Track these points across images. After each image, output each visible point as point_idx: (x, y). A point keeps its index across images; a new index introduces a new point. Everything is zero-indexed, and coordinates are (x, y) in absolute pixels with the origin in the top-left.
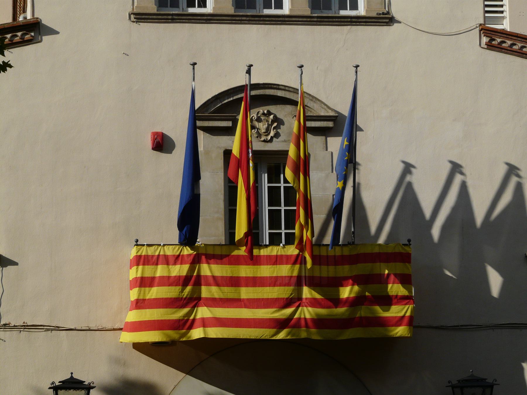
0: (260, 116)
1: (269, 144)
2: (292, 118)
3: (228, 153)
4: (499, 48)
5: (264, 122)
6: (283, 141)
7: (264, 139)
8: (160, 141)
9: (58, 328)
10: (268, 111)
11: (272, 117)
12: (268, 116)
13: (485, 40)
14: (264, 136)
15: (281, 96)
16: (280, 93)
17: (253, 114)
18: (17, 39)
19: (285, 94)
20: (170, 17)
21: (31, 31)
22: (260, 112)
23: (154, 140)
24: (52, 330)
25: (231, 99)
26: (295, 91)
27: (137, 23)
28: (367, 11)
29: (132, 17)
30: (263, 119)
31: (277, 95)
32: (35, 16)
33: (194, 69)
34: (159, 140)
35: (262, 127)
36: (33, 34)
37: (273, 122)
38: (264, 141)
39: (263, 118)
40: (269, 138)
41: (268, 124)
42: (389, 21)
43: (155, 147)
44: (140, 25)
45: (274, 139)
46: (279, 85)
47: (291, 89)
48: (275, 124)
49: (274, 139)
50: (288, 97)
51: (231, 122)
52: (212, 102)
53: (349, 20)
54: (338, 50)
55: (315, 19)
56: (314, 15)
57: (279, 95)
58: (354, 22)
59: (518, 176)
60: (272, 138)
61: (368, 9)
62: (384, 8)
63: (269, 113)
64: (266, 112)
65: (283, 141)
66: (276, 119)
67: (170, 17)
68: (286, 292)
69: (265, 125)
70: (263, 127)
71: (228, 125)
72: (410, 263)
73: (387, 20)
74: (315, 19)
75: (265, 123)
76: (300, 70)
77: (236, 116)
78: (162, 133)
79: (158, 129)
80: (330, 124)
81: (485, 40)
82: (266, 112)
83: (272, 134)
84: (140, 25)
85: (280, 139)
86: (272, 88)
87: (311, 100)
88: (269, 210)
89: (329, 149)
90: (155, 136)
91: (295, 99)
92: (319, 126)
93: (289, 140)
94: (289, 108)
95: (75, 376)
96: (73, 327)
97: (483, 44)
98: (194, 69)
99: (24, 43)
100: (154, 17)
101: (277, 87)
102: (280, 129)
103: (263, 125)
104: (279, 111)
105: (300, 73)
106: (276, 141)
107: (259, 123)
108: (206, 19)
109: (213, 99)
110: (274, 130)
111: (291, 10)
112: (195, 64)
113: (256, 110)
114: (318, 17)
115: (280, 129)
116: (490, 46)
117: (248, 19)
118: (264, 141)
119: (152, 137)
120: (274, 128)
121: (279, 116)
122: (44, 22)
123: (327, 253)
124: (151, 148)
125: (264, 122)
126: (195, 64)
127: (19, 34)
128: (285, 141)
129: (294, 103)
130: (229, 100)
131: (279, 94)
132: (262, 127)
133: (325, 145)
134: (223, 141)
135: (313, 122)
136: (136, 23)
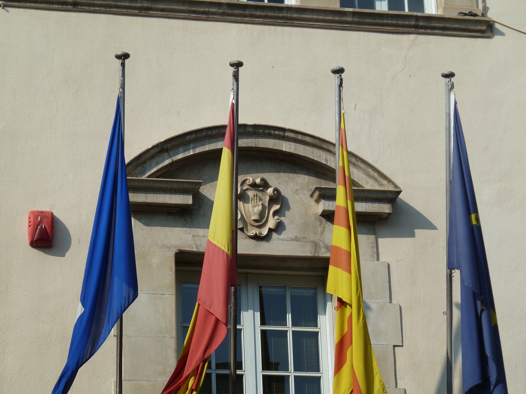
0: (247, 189)
1: (264, 244)
2: (309, 196)
5: (255, 201)
6: (292, 240)
7: (256, 233)
8: (48, 229)
10: (263, 180)
12: (262, 191)
14: (256, 229)
15: (288, 151)
16: (287, 147)
19: (295, 149)
22: (247, 182)
25: (191, 153)
27: (5, 8)
28: (445, 9)
30: (251, 198)
31: (281, 149)
34: (47, 227)
37: (273, 200)
38: (256, 238)
40: (265, 231)
41: (262, 205)
42: (487, 29)
43: (36, 240)
44: (8, 12)
46: (284, 130)
47: (307, 139)
48: (276, 207)
49: (275, 235)
50: (302, 155)
51: (191, 196)
52: (153, 157)
53: (413, 23)
54: (394, 76)
55: (349, 19)
56: (347, 9)
57: (284, 149)
58: (422, 27)
60: (270, 230)
61: (447, 6)
62: (476, 6)
63: (265, 185)
65: (292, 240)
69: (257, 205)
70: (253, 211)
71: (185, 203)
73: (484, 28)
74: (349, 19)
75: (257, 202)
76: (337, 78)
77: (200, 184)
79: (44, 207)
80: (385, 208)
82: (258, 181)
83: (271, 223)
84: (8, 12)
85: (284, 235)
86: (270, 136)
88: (264, 376)
89: (382, 258)
90: (38, 218)
91: (315, 159)
92: (363, 211)
93: (304, 238)
101: (282, 133)
102: (285, 216)
103: (254, 206)
105: (337, 82)
106: (278, 239)
107: (246, 205)
108: (140, 6)
109: (156, 150)
110: (276, 217)
115: (285, 216)
119: (32, 219)
120: (276, 213)
121: (285, 192)
125: (255, 201)
131: (284, 146)
133: (375, 250)
136: (3, 8)
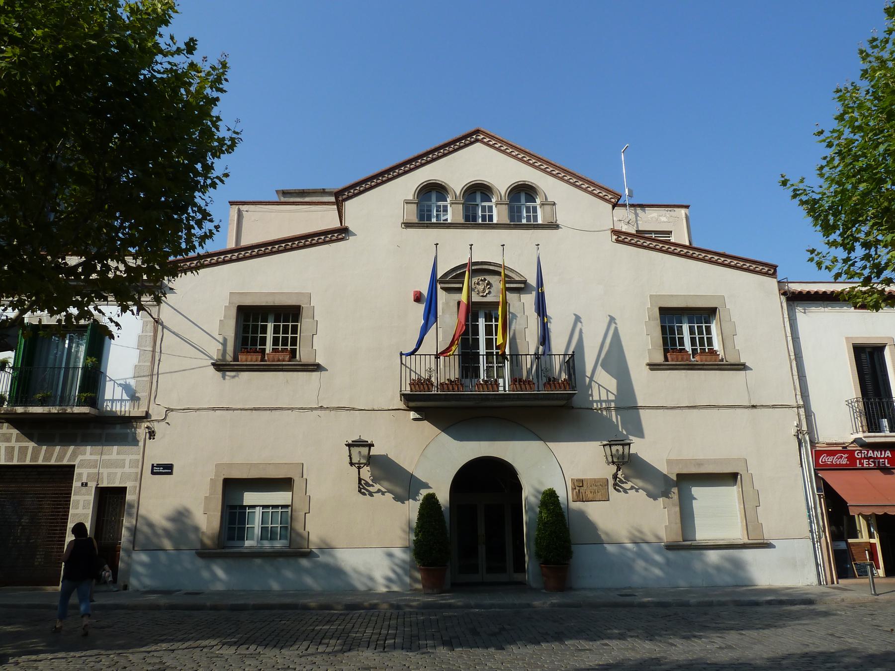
3: (459, 303)
4: (623, 242)
9: (353, 409)
11: (486, 281)
13: (615, 237)
16: (491, 268)
17: (475, 280)
18: (334, 238)
20: (426, 225)
21: (343, 233)
23: (415, 296)
24: (350, 410)
26: (500, 266)
29: (403, 225)
32: (346, 225)
33: (436, 247)
35: (481, 288)
36: (344, 235)
38: (482, 296)
39: (480, 283)
40: (485, 294)
45: (488, 295)
49: (488, 295)
52: (450, 273)
59: (616, 323)
63: (485, 280)
64: (483, 279)
66: (489, 283)
67: (426, 225)
68: (600, 485)
72: (299, 307)
74: (512, 226)
78: (420, 292)
80: (522, 286)
81: (615, 237)
82: (483, 279)
83: (487, 292)
85: (491, 295)
87: (511, 271)
94: (497, 277)
95: (362, 438)
96: (363, 409)
97: (614, 240)
98: (436, 247)
99: (338, 240)
100: (416, 225)
104: (489, 278)
111: (497, 221)
112: (437, 244)
113: (478, 278)
114: (514, 224)
116: (617, 241)
117: (472, 226)
118: (482, 296)
120: (488, 288)
122: (350, 229)
123: (608, 398)
124: (413, 300)
126: (437, 244)
127: (336, 235)
128: (495, 296)
129: (499, 273)
130: (461, 271)
132: (481, 288)
134: (456, 297)
135: (220, 514)
